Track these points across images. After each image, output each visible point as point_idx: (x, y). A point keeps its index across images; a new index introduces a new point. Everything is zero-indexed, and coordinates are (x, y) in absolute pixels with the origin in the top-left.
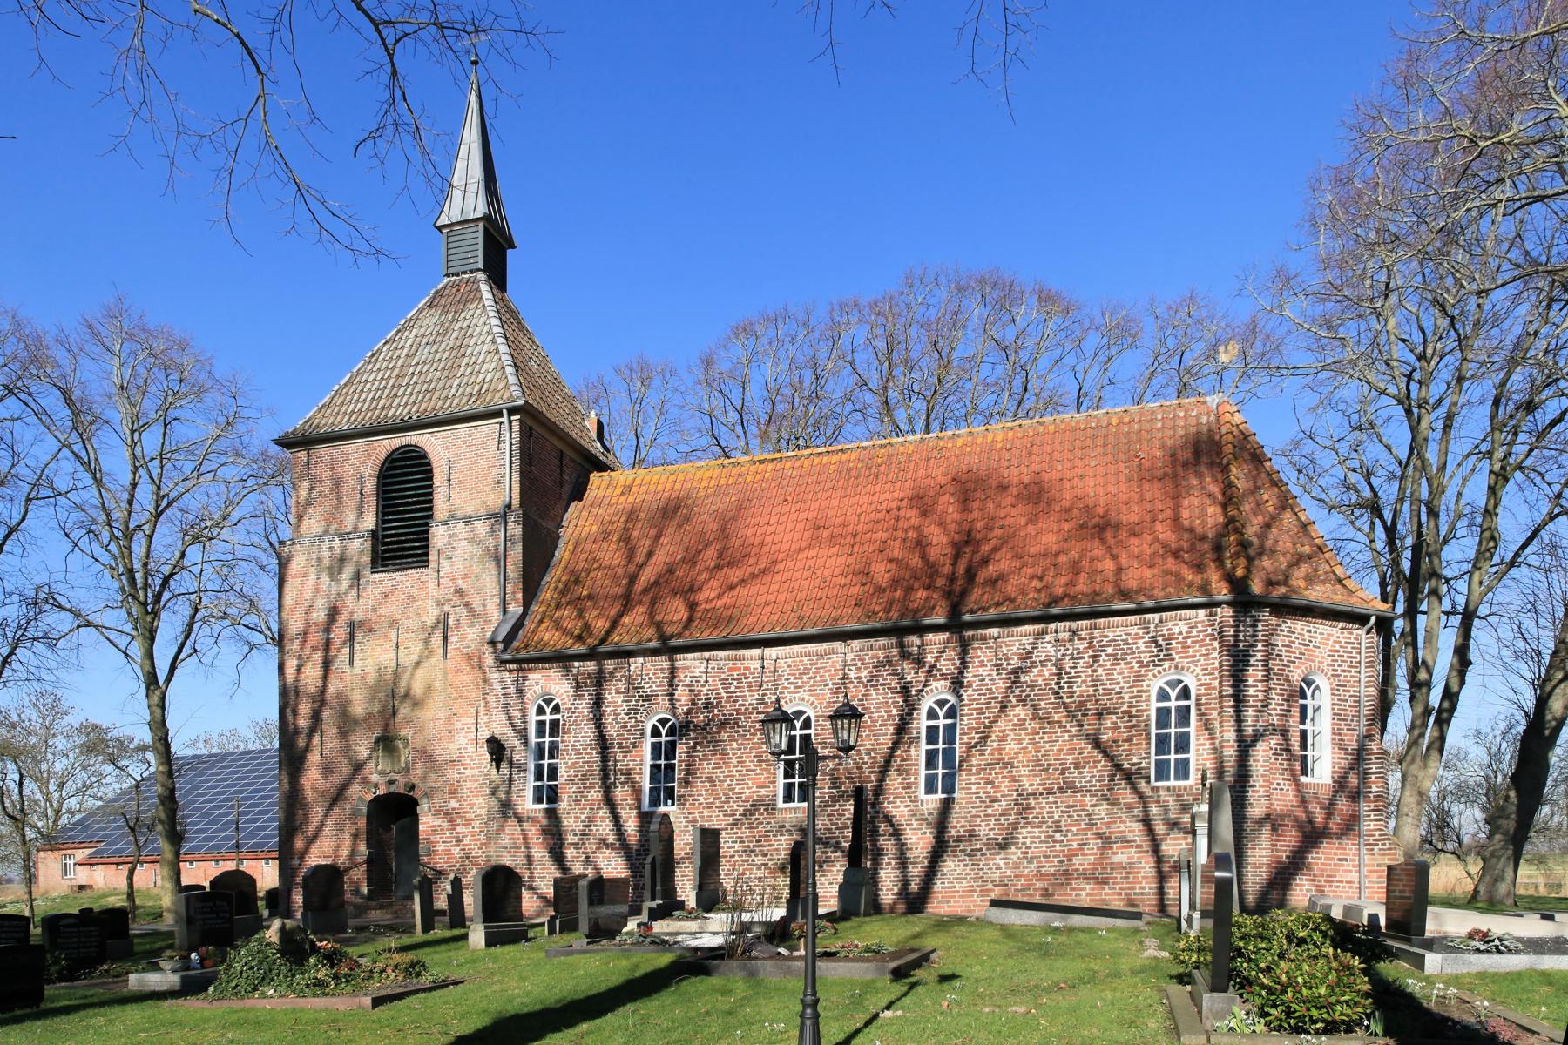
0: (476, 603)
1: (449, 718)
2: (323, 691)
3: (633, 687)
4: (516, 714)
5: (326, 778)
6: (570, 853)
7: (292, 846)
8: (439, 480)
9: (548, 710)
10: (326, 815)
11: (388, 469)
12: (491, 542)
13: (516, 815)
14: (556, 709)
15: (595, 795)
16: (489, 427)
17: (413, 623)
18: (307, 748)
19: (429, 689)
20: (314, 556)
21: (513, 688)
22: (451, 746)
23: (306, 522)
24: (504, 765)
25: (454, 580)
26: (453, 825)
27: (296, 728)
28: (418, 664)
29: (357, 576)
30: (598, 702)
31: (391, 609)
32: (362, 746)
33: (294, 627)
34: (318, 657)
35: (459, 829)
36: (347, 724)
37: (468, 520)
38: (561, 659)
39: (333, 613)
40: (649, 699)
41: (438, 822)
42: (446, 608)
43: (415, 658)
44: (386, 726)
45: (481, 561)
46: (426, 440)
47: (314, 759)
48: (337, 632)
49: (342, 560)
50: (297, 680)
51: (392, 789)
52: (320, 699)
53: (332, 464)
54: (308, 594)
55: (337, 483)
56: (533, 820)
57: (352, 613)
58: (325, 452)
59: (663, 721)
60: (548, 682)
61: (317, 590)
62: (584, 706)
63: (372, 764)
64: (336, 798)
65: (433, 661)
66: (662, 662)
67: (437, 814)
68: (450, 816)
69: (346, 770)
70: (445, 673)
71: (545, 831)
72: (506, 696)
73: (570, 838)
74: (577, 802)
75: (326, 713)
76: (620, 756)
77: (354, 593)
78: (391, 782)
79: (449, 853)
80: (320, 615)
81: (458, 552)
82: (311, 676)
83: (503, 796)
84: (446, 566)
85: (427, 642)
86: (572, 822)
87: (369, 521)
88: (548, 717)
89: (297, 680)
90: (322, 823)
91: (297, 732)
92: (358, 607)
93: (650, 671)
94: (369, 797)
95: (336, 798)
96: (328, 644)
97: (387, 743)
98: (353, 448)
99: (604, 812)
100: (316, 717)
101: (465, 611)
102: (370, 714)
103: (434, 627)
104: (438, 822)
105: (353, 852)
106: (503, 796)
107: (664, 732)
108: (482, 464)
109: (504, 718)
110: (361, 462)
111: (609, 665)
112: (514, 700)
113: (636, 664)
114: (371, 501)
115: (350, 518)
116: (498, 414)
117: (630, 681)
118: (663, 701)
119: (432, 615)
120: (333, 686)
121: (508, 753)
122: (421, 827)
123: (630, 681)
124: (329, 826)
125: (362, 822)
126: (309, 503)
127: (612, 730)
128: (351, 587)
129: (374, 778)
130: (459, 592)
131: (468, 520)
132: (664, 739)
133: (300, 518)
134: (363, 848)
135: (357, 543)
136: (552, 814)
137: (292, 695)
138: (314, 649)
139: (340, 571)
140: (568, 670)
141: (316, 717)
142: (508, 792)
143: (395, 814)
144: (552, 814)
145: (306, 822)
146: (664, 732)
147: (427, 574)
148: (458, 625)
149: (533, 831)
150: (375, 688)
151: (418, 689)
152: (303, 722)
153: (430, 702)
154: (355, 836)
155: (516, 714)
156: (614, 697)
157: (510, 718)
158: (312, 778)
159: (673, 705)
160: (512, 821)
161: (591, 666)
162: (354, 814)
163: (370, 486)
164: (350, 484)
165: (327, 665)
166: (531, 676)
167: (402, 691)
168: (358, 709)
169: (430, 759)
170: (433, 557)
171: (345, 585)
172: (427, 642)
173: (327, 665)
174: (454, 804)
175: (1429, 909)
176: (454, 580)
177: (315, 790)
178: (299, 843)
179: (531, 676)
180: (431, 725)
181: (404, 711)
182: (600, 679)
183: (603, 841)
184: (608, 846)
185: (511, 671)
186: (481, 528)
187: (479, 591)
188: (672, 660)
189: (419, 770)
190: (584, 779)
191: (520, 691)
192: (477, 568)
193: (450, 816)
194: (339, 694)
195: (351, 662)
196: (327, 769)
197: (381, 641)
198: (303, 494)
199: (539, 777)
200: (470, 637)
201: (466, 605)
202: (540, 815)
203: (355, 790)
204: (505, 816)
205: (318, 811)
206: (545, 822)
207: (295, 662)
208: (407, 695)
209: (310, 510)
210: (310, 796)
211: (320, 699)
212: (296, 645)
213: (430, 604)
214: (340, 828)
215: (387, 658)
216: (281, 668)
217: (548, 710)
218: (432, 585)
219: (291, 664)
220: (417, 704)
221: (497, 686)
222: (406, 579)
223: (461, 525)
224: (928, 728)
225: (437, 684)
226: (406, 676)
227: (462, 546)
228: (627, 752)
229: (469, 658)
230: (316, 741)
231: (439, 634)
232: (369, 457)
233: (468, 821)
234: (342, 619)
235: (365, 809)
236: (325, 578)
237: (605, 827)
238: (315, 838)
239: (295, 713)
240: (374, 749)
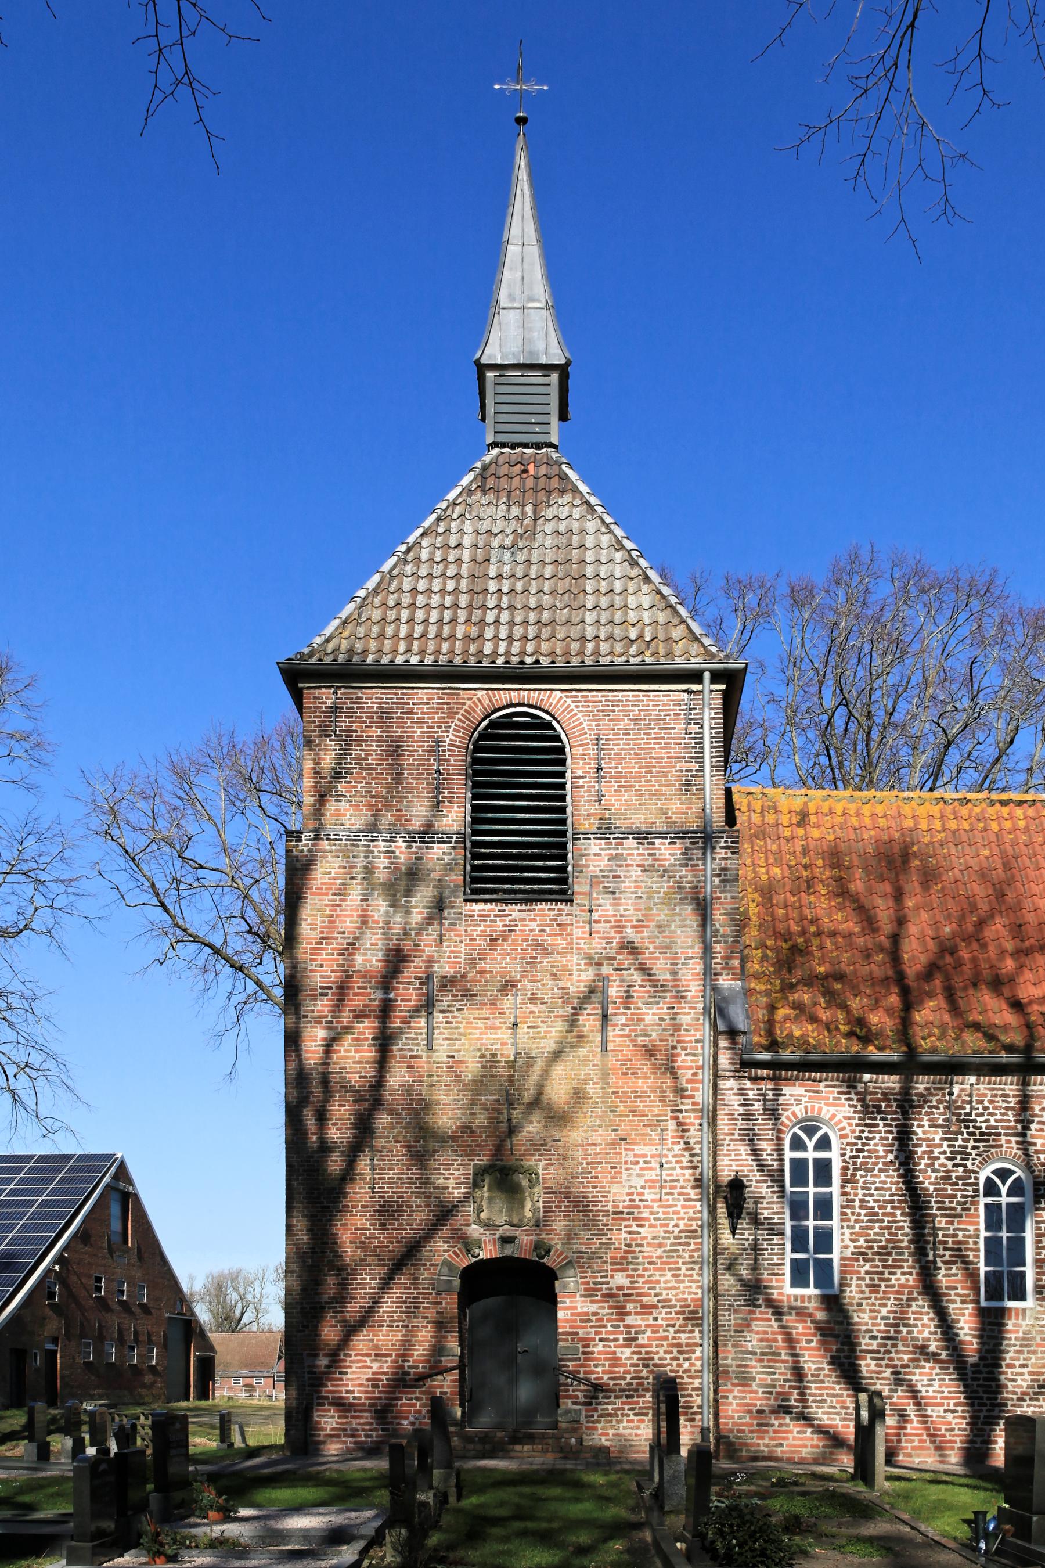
0: (661, 968)
1: (613, 1144)
2: (379, 1083)
3: (960, 1118)
4: (767, 1148)
5: (383, 1227)
6: (867, 1366)
7: (316, 1333)
8: (577, 765)
9: (810, 1144)
10: (385, 1285)
11: (482, 737)
12: (686, 875)
13: (770, 1303)
14: (824, 1144)
15: (905, 1277)
16: (674, 694)
17: (547, 988)
18: (348, 1174)
19: (579, 1096)
20: (360, 863)
21: (758, 1106)
22: (615, 1189)
23: (331, 806)
24: (744, 1224)
25: (619, 927)
26: (622, 1314)
27: (322, 1140)
28: (557, 1055)
29: (439, 906)
30: (904, 1137)
31: (503, 962)
32: (452, 1178)
33: (321, 971)
34: (367, 1028)
35: (629, 1320)
36: (423, 1144)
37: (643, 836)
38: (848, 1069)
39: (397, 959)
40: (987, 1139)
41: (594, 1308)
42: (606, 970)
43: (549, 1044)
44: (499, 1149)
45: (667, 900)
46: (558, 702)
47: (359, 1193)
48: (394, 993)
49: (412, 875)
50: (326, 1063)
51: (509, 1250)
52: (372, 1097)
53: (384, 716)
54: (348, 923)
55: (395, 749)
56: (801, 1313)
57: (430, 963)
58: (374, 696)
59: (1003, 1174)
60: (824, 1105)
61: (364, 920)
62: (881, 1141)
63: (470, 1208)
64: (405, 1258)
65: (583, 1051)
66: (1009, 1085)
67: (590, 1294)
68: (618, 1301)
69: (419, 1217)
70: (605, 1075)
71: (824, 1331)
72: (748, 1116)
73: (865, 1343)
74: (874, 1288)
75: (383, 1120)
76: (941, 1222)
77: (433, 931)
78: (506, 1240)
79: (615, 1360)
80: (370, 958)
81: (628, 885)
82: (354, 1058)
83: (745, 1273)
84: (605, 906)
85: (572, 1022)
86: (869, 1318)
87: (455, 817)
88: (811, 1155)
89: (326, 1063)
90: (376, 1302)
91: (325, 1148)
92: (447, 952)
93: (989, 1098)
94: (465, 1262)
95: (405, 1258)
96: (386, 1010)
97: (503, 1175)
98: (423, 693)
99: (921, 1304)
100: (364, 1126)
101: (637, 977)
102: (467, 1129)
103: (585, 999)
104: (594, 1308)
105: (438, 1350)
106: (745, 1273)
107: (1004, 1190)
108: (658, 751)
109: (744, 1151)
110: (440, 722)
111: (922, 1084)
112: (763, 1125)
113: (964, 1085)
114: (459, 784)
115: (418, 811)
116: (696, 677)
117: (953, 1108)
118: (1010, 1145)
119: (579, 979)
120: (397, 1078)
121: (749, 1205)
122: (561, 1315)
123: (953, 1108)
124: (388, 1305)
125: (450, 1303)
126: (337, 776)
127: (928, 1181)
128: (429, 921)
129: (474, 1231)
130: (630, 948)
131: (643, 836)
132: (1004, 1200)
133: (322, 798)
134: (453, 1344)
135: (438, 850)
136: (833, 1303)
137: (316, 1092)
138: (359, 1016)
139: (409, 893)
140: (851, 1085)
141: (364, 1126)
142: (755, 1268)
143: (511, 1293)
144: (833, 1303)
145: (342, 1298)
146: (1004, 1190)
147: (572, 914)
148: (628, 998)
149: (800, 1328)
150: (478, 1087)
151: (558, 1092)
152: (339, 1131)
153: (580, 1118)
154: (440, 1325)
155: (767, 1148)
156: (926, 1131)
157: (755, 1152)
158: (356, 1227)
159: (1025, 1151)
160: (763, 1311)
161: (891, 1082)
162: (439, 1288)
163: (456, 762)
164: (416, 751)
165: (384, 1042)
166: (786, 1090)
167: (528, 1096)
168: (447, 1116)
169: (580, 1206)
170: (579, 886)
171: (417, 917)
172: (572, 1022)
173: (384, 1042)
174: (620, 1279)
175: (283, 1441)
176: (619, 927)
177: (363, 1246)
178: (329, 1332)
179: (786, 1090)
180: (580, 1153)
181: (533, 1127)
182: (907, 1104)
183: (922, 1350)
184: (934, 1357)
185: (755, 1079)
186: (668, 852)
187: (666, 948)
188: (1025, 1083)
189: (559, 1226)
190: (884, 1253)
191: (773, 1113)
192: (661, 915)
193: (618, 1301)
194: (408, 1091)
195: (429, 1047)
196: (387, 1212)
197: (485, 1013)
198: (328, 759)
199: (799, 1241)
200: (649, 1019)
201: (643, 969)
202: (812, 1305)
203: (441, 1251)
204: (752, 1303)
205: (368, 1280)
206: (820, 1316)
207: (321, 1033)
208: (536, 1102)
209: (341, 787)
210: (349, 1251)
211: (372, 1097)
212: (322, 1006)
213: (574, 960)
214: (412, 1309)
215: (501, 1041)
216: (293, 1041)
217: (810, 1144)
218: (578, 932)
219: (314, 1038)
220: (558, 1118)
221: (733, 1101)
222: (532, 919)
223: (631, 843)
224: (793, 1161)
225: (590, 1089)
226: (536, 1072)
227: (632, 877)
228: (953, 1216)
229: (650, 1052)
230: (363, 1165)
231: (592, 1010)
232: (452, 714)
233: (647, 1309)
234: (413, 970)
235: (457, 1282)
236: (380, 907)
237: (924, 1327)
238: (362, 1322)
239: (322, 1117)
240: (476, 1185)
